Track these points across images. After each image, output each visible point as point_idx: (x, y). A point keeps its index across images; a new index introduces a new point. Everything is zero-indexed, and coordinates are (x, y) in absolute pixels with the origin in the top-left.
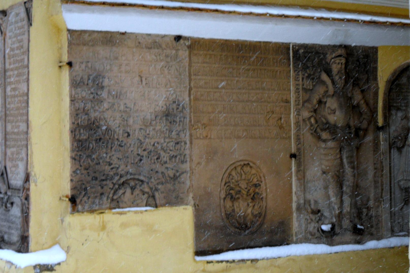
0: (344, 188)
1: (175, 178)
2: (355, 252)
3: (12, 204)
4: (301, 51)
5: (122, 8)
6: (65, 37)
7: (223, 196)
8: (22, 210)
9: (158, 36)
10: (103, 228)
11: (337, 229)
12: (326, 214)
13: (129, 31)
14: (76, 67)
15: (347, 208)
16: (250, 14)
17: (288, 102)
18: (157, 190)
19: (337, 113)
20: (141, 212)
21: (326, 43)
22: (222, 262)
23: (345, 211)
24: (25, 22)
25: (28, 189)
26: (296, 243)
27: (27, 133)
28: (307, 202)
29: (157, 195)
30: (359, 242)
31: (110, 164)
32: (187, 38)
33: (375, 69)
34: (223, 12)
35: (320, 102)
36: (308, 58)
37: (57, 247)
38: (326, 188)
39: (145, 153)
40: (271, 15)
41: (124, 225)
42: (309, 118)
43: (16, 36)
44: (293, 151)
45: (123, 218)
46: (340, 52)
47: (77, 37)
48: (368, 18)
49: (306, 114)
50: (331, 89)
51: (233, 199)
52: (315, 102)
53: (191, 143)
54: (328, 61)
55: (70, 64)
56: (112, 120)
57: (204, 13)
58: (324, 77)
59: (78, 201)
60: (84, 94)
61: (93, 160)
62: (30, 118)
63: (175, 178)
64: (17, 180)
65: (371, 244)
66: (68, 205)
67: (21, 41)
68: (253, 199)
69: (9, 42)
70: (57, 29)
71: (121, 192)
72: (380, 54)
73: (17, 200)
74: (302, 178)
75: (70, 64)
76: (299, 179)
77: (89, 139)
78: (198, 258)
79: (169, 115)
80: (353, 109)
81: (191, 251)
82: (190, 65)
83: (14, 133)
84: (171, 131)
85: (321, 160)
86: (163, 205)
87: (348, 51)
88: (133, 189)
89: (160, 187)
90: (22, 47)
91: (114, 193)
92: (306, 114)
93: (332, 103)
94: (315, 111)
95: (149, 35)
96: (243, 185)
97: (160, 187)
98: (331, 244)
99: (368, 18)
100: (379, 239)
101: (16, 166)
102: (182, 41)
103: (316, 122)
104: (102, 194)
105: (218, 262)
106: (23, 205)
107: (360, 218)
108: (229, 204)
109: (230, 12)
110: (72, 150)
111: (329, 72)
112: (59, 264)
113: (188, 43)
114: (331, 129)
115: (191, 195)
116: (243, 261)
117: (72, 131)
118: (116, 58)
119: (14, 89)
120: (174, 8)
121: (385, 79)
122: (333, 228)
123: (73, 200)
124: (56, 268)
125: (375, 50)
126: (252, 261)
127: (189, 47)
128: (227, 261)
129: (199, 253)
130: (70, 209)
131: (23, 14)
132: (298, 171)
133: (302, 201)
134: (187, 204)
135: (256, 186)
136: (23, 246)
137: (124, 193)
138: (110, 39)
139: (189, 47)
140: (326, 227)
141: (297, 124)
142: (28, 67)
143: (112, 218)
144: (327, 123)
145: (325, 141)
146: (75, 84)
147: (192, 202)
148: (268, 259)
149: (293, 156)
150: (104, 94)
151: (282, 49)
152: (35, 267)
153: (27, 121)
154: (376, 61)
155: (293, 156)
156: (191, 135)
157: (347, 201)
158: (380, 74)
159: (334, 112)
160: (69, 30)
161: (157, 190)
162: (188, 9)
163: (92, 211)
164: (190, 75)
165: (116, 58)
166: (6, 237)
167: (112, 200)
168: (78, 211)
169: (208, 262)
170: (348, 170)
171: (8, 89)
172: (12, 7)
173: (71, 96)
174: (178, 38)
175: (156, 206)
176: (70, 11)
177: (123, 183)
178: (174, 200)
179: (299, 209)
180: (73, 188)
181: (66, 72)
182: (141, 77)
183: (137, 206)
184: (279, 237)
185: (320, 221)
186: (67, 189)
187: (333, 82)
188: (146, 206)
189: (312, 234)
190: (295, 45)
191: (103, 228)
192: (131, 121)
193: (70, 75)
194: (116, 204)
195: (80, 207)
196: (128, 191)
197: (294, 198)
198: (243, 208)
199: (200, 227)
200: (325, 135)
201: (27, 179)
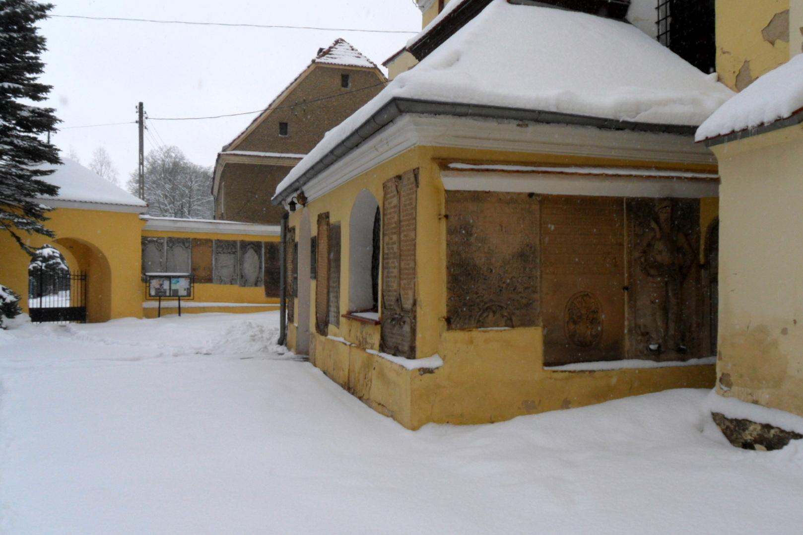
0: (670, 315)
1: (528, 305)
2: (677, 367)
3: (404, 322)
4: (633, 203)
5: (486, 173)
6: (443, 194)
7: (567, 319)
8: (411, 328)
9: (515, 193)
10: (471, 342)
11: (663, 350)
12: (654, 335)
13: (492, 190)
14: (451, 219)
15: (671, 332)
16: (590, 174)
17: (621, 245)
18: (513, 314)
19: (664, 254)
20: (501, 331)
21: (656, 196)
22: (565, 371)
23: (670, 334)
24: (414, 185)
25: (415, 312)
26: (628, 358)
27: (414, 269)
28: (637, 326)
29: (514, 318)
30: (683, 360)
31: (477, 293)
32: (538, 195)
33: (698, 217)
34: (567, 174)
35: (649, 245)
36: (638, 209)
37: (436, 356)
38: (654, 314)
39: (504, 285)
40: (607, 175)
41: (486, 341)
42: (640, 258)
43: (408, 194)
44: (626, 283)
45: (487, 335)
46: (665, 203)
47: (453, 197)
48: (689, 175)
49: (636, 254)
50: (658, 235)
51: (575, 323)
52: (645, 244)
53: (541, 278)
54: (656, 210)
55: (446, 217)
56: (480, 260)
57: (552, 176)
58: (653, 225)
59: (452, 321)
60: (457, 239)
61: (463, 290)
62: (417, 258)
63: (528, 305)
64: (408, 305)
65: (693, 361)
66: (444, 324)
67: (411, 199)
68: (592, 323)
69: (403, 199)
70: (437, 189)
71: (485, 315)
72: (702, 204)
73: (407, 320)
74: (634, 308)
75: (446, 217)
76: (630, 307)
77: (461, 274)
78: (546, 368)
79: (524, 256)
80: (675, 248)
81: (540, 362)
82: (541, 217)
83: (406, 269)
84: (525, 269)
85: (649, 295)
86: (519, 326)
87: (673, 202)
88: (494, 312)
89: (516, 311)
90: (411, 204)
91: (480, 316)
92: (636, 254)
93: (659, 246)
94: (645, 252)
95: (508, 193)
96: (583, 311)
97: (516, 311)
98: (658, 360)
99: (689, 175)
100: (700, 357)
101: (407, 294)
102: (534, 197)
103: (646, 260)
104: (471, 316)
105: (562, 371)
106: (412, 323)
107: (683, 340)
108: (572, 327)
109: (572, 174)
110: (448, 282)
111: (657, 221)
112: (437, 368)
113: (540, 198)
114: (658, 266)
115: (541, 319)
116: (582, 371)
117: (448, 268)
118: (482, 211)
119: (406, 236)
120: (527, 172)
121: (707, 225)
122: (659, 347)
123: (448, 320)
124: (436, 371)
125: (697, 201)
126: (590, 372)
127: (540, 202)
128: (570, 372)
129: (547, 364)
130: (446, 327)
131: (412, 179)
132: (630, 300)
133: (633, 325)
134: (537, 325)
135: (594, 312)
136: (411, 354)
137: (487, 316)
138: (477, 197)
139: (540, 202)
140: (652, 347)
141: (629, 262)
142: (415, 219)
143: (477, 335)
144: (655, 261)
145: (652, 276)
146: (450, 232)
147: (542, 324)
148: (603, 371)
149: (626, 288)
150: (472, 239)
151: (618, 201)
152: (419, 370)
153: (415, 260)
154: (698, 210)
155: (626, 288)
156: (541, 272)
157: (672, 325)
158: (701, 221)
159: (660, 252)
160: (447, 191)
161: (513, 314)
162: (538, 172)
163: (462, 329)
164: (540, 225)
165: (482, 211)
166: (400, 347)
167: (479, 321)
168: (452, 329)
169: (554, 372)
170: (673, 301)
171: (402, 235)
172: (405, 173)
173: (447, 241)
174: (531, 195)
175: (513, 327)
176: (447, 176)
177: (487, 309)
178: (527, 322)
179: (630, 331)
180: (448, 312)
181: (444, 221)
182: (501, 226)
183: (498, 326)
184: (615, 353)
185: (648, 342)
186: (444, 311)
187: (660, 228)
188: (506, 326)
189: (642, 352)
190: (628, 199)
191: (471, 342)
192: (493, 260)
193: (447, 225)
194: (481, 324)
195: (453, 326)
196: (491, 315)
197: (626, 323)
198: (584, 330)
199: (549, 343)
200: (652, 272)
201: (415, 304)
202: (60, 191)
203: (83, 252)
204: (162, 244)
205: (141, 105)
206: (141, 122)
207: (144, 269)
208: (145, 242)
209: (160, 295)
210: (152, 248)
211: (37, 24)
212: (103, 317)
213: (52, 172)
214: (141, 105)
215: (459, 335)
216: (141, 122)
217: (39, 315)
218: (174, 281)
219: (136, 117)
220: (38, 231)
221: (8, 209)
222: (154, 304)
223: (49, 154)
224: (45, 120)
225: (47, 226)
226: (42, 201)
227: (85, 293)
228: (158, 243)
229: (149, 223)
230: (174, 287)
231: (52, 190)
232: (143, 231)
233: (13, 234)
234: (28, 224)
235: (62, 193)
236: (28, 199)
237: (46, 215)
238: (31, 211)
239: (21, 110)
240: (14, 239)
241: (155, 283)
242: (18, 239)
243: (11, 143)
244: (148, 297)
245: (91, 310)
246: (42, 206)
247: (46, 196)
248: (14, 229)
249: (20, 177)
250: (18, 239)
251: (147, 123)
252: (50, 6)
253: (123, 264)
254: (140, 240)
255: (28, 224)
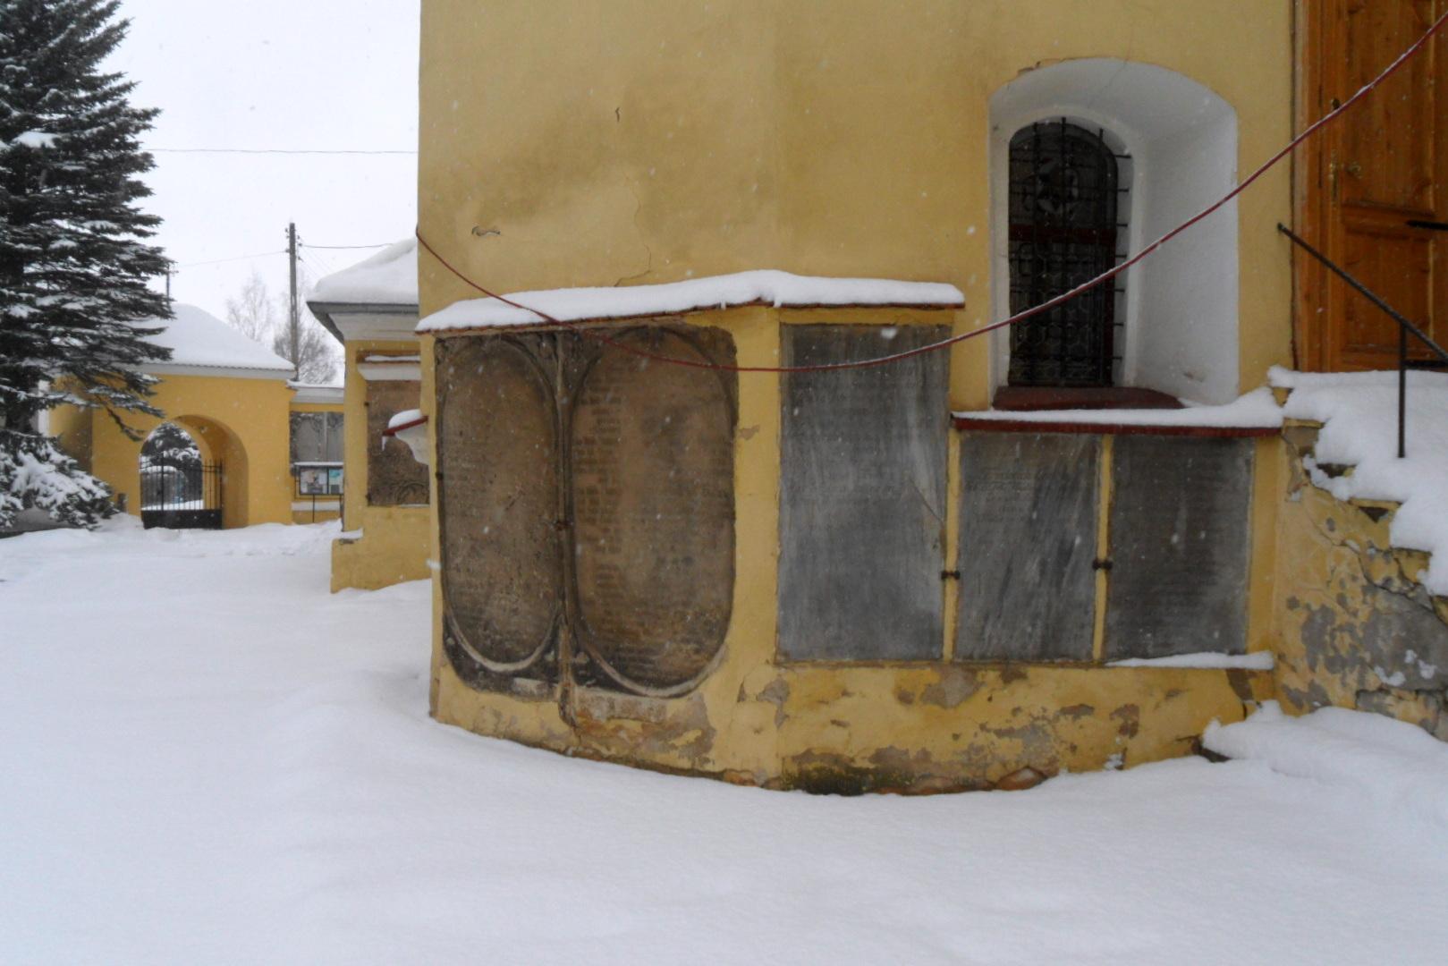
143: (397, 511)
163: (383, 505)
202: (173, 354)
203: (218, 437)
204: (320, 422)
205: (292, 227)
206: (292, 251)
207: (294, 456)
208: (296, 420)
209: (314, 494)
210: (306, 429)
211: (142, 136)
212: (240, 523)
213: (161, 330)
214: (292, 227)
215: (378, 512)
216: (292, 251)
217: (151, 520)
218: (333, 473)
219: (286, 244)
220: (143, 409)
221: (105, 381)
222: (307, 506)
223: (159, 305)
224: (154, 262)
225: (152, 403)
226: (147, 370)
227: (220, 490)
228: (315, 420)
229: (300, 393)
230: (332, 482)
231: (163, 353)
232: (291, 404)
233: (112, 414)
234: (127, 400)
235: (178, 356)
236: (130, 368)
237: (152, 389)
238: (134, 383)
239: (122, 252)
240: (113, 420)
241: (306, 477)
242: (118, 420)
243: (107, 297)
244: (298, 496)
245: (228, 515)
246: (146, 377)
247: (157, 360)
248: (111, 406)
249: (121, 341)
250: (118, 420)
251: (300, 252)
252: (156, 112)
253: (265, 451)
254: (287, 419)
255: (127, 400)
